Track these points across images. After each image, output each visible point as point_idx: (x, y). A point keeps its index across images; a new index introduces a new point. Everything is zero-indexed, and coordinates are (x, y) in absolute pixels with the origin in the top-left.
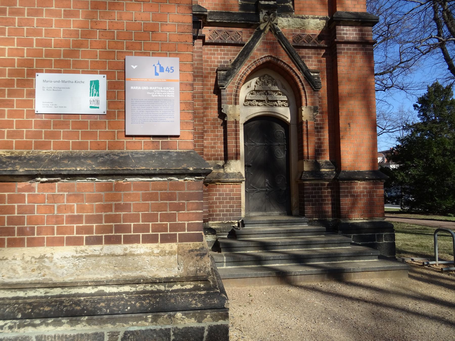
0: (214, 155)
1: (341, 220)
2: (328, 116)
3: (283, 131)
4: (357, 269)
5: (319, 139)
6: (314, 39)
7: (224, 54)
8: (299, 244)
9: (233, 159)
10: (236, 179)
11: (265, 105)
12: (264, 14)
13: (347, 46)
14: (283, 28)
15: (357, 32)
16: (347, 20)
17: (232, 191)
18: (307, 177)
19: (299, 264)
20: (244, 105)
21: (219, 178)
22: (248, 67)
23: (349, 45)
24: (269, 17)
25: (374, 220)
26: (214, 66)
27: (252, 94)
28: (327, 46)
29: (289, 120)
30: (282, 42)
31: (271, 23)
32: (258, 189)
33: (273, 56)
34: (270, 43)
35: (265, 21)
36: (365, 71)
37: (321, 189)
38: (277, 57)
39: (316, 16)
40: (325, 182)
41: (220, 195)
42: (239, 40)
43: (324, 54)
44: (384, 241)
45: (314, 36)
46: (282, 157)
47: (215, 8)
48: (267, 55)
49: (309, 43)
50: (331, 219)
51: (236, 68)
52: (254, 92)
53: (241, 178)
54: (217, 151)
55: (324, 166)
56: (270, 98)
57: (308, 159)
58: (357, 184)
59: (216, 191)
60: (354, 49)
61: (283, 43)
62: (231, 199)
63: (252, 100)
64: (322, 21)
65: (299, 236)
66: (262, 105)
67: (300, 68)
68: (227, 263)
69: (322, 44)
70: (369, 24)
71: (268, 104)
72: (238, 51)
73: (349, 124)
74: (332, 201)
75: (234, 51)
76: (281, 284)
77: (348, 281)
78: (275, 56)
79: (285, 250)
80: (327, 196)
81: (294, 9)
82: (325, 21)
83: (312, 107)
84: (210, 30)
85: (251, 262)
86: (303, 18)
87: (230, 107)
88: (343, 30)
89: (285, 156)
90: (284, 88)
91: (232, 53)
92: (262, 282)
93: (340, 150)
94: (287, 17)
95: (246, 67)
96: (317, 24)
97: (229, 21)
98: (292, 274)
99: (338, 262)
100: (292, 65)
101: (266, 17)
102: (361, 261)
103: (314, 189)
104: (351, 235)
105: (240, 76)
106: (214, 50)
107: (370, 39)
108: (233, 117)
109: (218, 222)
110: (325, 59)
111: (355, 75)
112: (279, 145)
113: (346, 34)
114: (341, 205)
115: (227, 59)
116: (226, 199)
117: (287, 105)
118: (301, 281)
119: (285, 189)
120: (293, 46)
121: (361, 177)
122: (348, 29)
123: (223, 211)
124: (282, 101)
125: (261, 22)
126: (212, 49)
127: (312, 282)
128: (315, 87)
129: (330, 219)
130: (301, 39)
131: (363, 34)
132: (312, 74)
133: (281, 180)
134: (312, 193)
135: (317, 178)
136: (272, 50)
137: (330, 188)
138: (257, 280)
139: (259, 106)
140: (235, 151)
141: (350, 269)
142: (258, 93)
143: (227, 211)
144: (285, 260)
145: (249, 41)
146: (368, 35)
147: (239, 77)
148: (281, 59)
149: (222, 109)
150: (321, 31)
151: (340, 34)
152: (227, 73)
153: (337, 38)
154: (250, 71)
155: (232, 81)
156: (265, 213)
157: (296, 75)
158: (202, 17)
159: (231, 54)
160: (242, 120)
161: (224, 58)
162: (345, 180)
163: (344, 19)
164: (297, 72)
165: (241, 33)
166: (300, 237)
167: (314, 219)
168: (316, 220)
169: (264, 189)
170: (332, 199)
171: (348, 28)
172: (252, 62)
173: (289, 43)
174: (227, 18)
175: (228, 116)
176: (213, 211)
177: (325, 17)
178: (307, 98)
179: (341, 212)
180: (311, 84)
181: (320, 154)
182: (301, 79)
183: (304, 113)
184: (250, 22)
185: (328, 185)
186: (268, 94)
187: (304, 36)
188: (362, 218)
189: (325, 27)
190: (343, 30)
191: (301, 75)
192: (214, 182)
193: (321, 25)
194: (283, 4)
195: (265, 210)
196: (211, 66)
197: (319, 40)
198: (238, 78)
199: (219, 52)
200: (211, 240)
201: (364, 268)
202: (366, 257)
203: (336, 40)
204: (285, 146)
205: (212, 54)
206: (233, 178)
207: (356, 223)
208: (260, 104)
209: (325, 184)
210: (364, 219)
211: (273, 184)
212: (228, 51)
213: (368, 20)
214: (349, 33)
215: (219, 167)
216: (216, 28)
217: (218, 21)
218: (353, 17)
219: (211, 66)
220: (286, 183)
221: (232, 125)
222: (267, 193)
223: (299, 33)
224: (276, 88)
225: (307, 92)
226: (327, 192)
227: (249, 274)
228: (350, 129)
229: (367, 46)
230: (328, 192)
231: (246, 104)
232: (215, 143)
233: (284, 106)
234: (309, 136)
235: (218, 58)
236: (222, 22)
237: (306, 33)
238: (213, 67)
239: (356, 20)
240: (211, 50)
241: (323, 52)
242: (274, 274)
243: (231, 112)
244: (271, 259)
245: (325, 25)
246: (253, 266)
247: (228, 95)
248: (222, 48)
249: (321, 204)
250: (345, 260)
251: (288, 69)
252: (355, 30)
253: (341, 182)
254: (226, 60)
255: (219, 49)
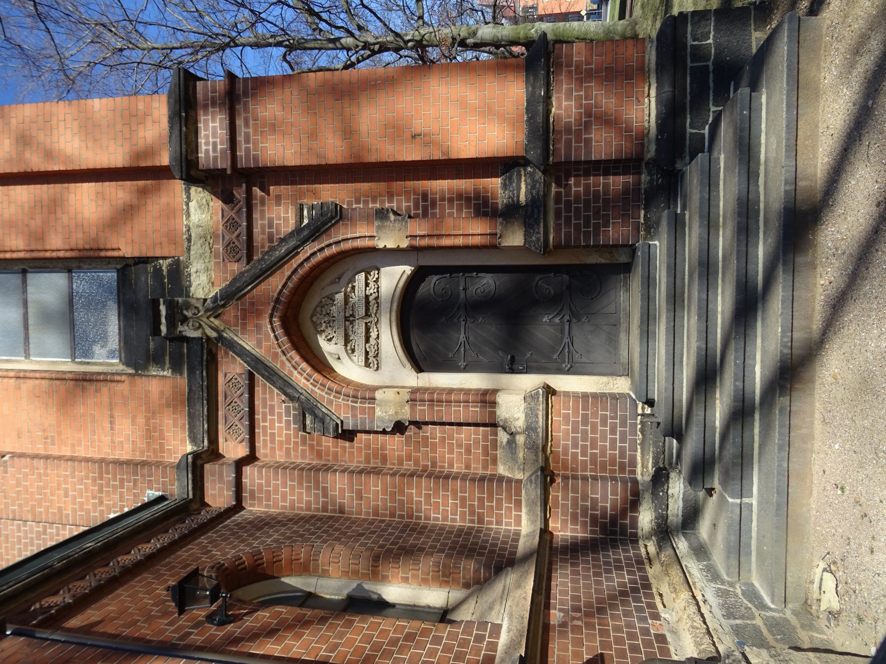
0: (485, 448)
1: (649, 156)
2: (396, 181)
3: (434, 279)
4: (787, 171)
5: (451, 200)
6: (232, 214)
7: (272, 413)
8: (705, 296)
9: (495, 412)
10: (539, 410)
11: (376, 324)
12: (186, 328)
13: (240, 141)
14: (213, 283)
15: (210, 117)
16: (184, 146)
17: (566, 417)
18: (538, 239)
19: (760, 305)
20: (377, 369)
21: (538, 448)
22: (296, 369)
23: (238, 139)
24: (191, 318)
25: (653, 65)
26: (296, 436)
27: (353, 351)
28: (244, 185)
29: (408, 269)
30: (241, 291)
31: (201, 316)
32: (566, 340)
33: (270, 312)
34: (244, 318)
35: (200, 326)
36: (291, 94)
37: (568, 204)
38: (272, 304)
39: (185, 207)
40: (553, 193)
41: (575, 445)
42: (244, 382)
43: (262, 189)
44: (710, 41)
45: (225, 214)
46: (491, 282)
47: (181, 427)
48: (269, 326)
49: (240, 226)
50: (643, 176)
51: (297, 396)
52: (349, 348)
53: (538, 398)
54: (476, 441)
55: (514, 195)
56: (360, 313)
57: (496, 234)
58: (559, 116)
59: (566, 452)
60: (247, 125)
61: (243, 289)
62: (585, 421)
63: (367, 353)
64: (192, 196)
65: (684, 278)
66: (375, 330)
67: (293, 252)
68: (744, 494)
69: (240, 194)
70: (191, 88)
71: (373, 315)
72: (523, 577)
73: (414, 137)
74: (600, 175)
75: (264, 393)
76: (812, 381)
77: (819, 196)
78: (271, 307)
79: (719, 331)
80: (587, 187)
81: (173, 257)
82: (193, 189)
83: (376, 223)
84: (226, 441)
85: (747, 434)
86: (189, 240)
87: (380, 413)
88: (207, 151)
89: (490, 275)
90: (340, 279)
91: (268, 396)
92: (804, 431)
93: (476, 158)
94: (190, 274)
95: (295, 372)
96: (200, 207)
97: (205, 402)
98: (786, 354)
99: (762, 206)
100: (287, 271)
101: (190, 324)
102: (763, 140)
103: (568, 220)
104: (688, 135)
105: (315, 386)
106: (265, 435)
107: (222, 87)
108: (402, 407)
109: (639, 454)
110: (271, 188)
111: (299, 118)
112: (465, 289)
113: (215, 144)
114: (609, 158)
115: (281, 409)
116: (585, 432)
117: (377, 272)
118: (811, 328)
119: (566, 277)
120: (248, 263)
121: (541, 108)
122: (203, 141)
123: (613, 441)
124: (367, 285)
125: (202, 334)
126: (262, 438)
127: (813, 297)
128: (332, 218)
129: (645, 178)
130: (234, 243)
131: (214, 104)
132: (306, 221)
133: (546, 287)
134: (577, 226)
135: (542, 216)
136: (259, 314)
137: (567, 179)
138: (796, 443)
139: (378, 335)
140: (477, 407)
141: (786, 191)
142: (351, 338)
143: (613, 432)
144: (747, 349)
145: (241, 361)
146: (214, 91)
147: (316, 390)
148: (276, 295)
149: (384, 429)
150: (213, 197)
151: (215, 158)
152: (310, 414)
153: (224, 167)
154: (304, 365)
155: (325, 404)
156: (622, 325)
157: (307, 259)
158: (199, 462)
159: (272, 399)
160: (412, 379)
161: (280, 414)
162: (548, 147)
163: (184, 153)
164: (301, 257)
165: (228, 375)
166: (687, 277)
167: (642, 221)
168: (645, 215)
169: (567, 327)
170: (594, 175)
171: (202, 141)
172: (284, 358)
173: (242, 274)
174: (198, 407)
175: (399, 418)
176: (613, 463)
177: (185, 189)
178: (358, 235)
179: (629, 156)
180: (326, 227)
181: (486, 200)
182: (315, 249)
183: (391, 245)
184: (205, 358)
185: (559, 185)
186: (352, 315)
187: (227, 238)
188: (646, 100)
189: (204, 188)
190: (207, 151)
191: (309, 249)
192: (546, 459)
193: (202, 199)
194: (166, 281)
195: (616, 325)
196: (298, 442)
197: (233, 202)
198: (318, 391)
199: (267, 424)
200: (682, 486)
201: (786, 151)
202: (753, 128)
203: (229, 172)
204: (467, 275)
205: (273, 441)
206: (537, 416)
207: (657, 117)
208: (373, 335)
209: (556, 192)
210: (649, 95)
211: (553, 302)
212: (264, 406)
213: (182, 93)
214: (213, 138)
215: (512, 443)
216: (221, 427)
217: (206, 426)
218: (177, 132)
219: (296, 443)
220: (552, 275)
221: (420, 410)
222: (574, 320)
223: (220, 247)
224: (340, 297)
225: (345, 237)
226: (576, 186)
227: (780, 466)
228: (425, 135)
229: (237, 92)
230: (577, 185)
231: (376, 366)
232: (460, 446)
233: (378, 279)
234: (443, 233)
235: (280, 428)
236: (208, 416)
237: (221, 232)
238: (298, 438)
239: (183, 124)
240: (265, 441)
241: (256, 191)
242: (783, 401)
243: (391, 412)
244: (741, 387)
245: (200, 189)
246: (757, 431)
247: (354, 416)
248: (260, 416)
249: (606, 201)
250: (758, 186)
251: (295, 278)
252: (206, 122)
253: (551, 159)
254: (283, 411)
255: (261, 424)
